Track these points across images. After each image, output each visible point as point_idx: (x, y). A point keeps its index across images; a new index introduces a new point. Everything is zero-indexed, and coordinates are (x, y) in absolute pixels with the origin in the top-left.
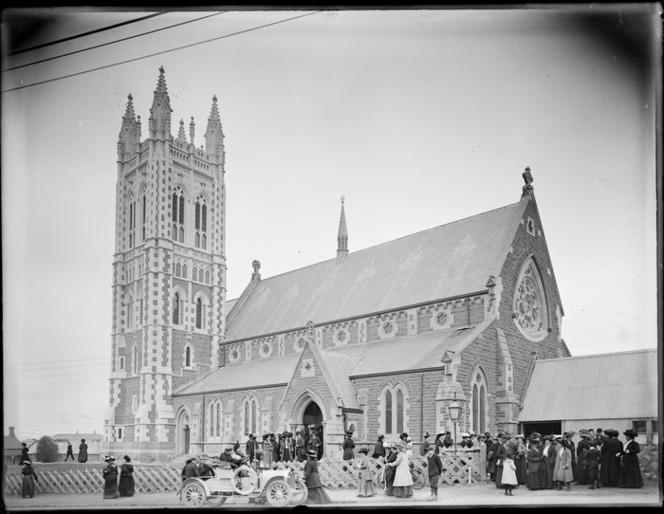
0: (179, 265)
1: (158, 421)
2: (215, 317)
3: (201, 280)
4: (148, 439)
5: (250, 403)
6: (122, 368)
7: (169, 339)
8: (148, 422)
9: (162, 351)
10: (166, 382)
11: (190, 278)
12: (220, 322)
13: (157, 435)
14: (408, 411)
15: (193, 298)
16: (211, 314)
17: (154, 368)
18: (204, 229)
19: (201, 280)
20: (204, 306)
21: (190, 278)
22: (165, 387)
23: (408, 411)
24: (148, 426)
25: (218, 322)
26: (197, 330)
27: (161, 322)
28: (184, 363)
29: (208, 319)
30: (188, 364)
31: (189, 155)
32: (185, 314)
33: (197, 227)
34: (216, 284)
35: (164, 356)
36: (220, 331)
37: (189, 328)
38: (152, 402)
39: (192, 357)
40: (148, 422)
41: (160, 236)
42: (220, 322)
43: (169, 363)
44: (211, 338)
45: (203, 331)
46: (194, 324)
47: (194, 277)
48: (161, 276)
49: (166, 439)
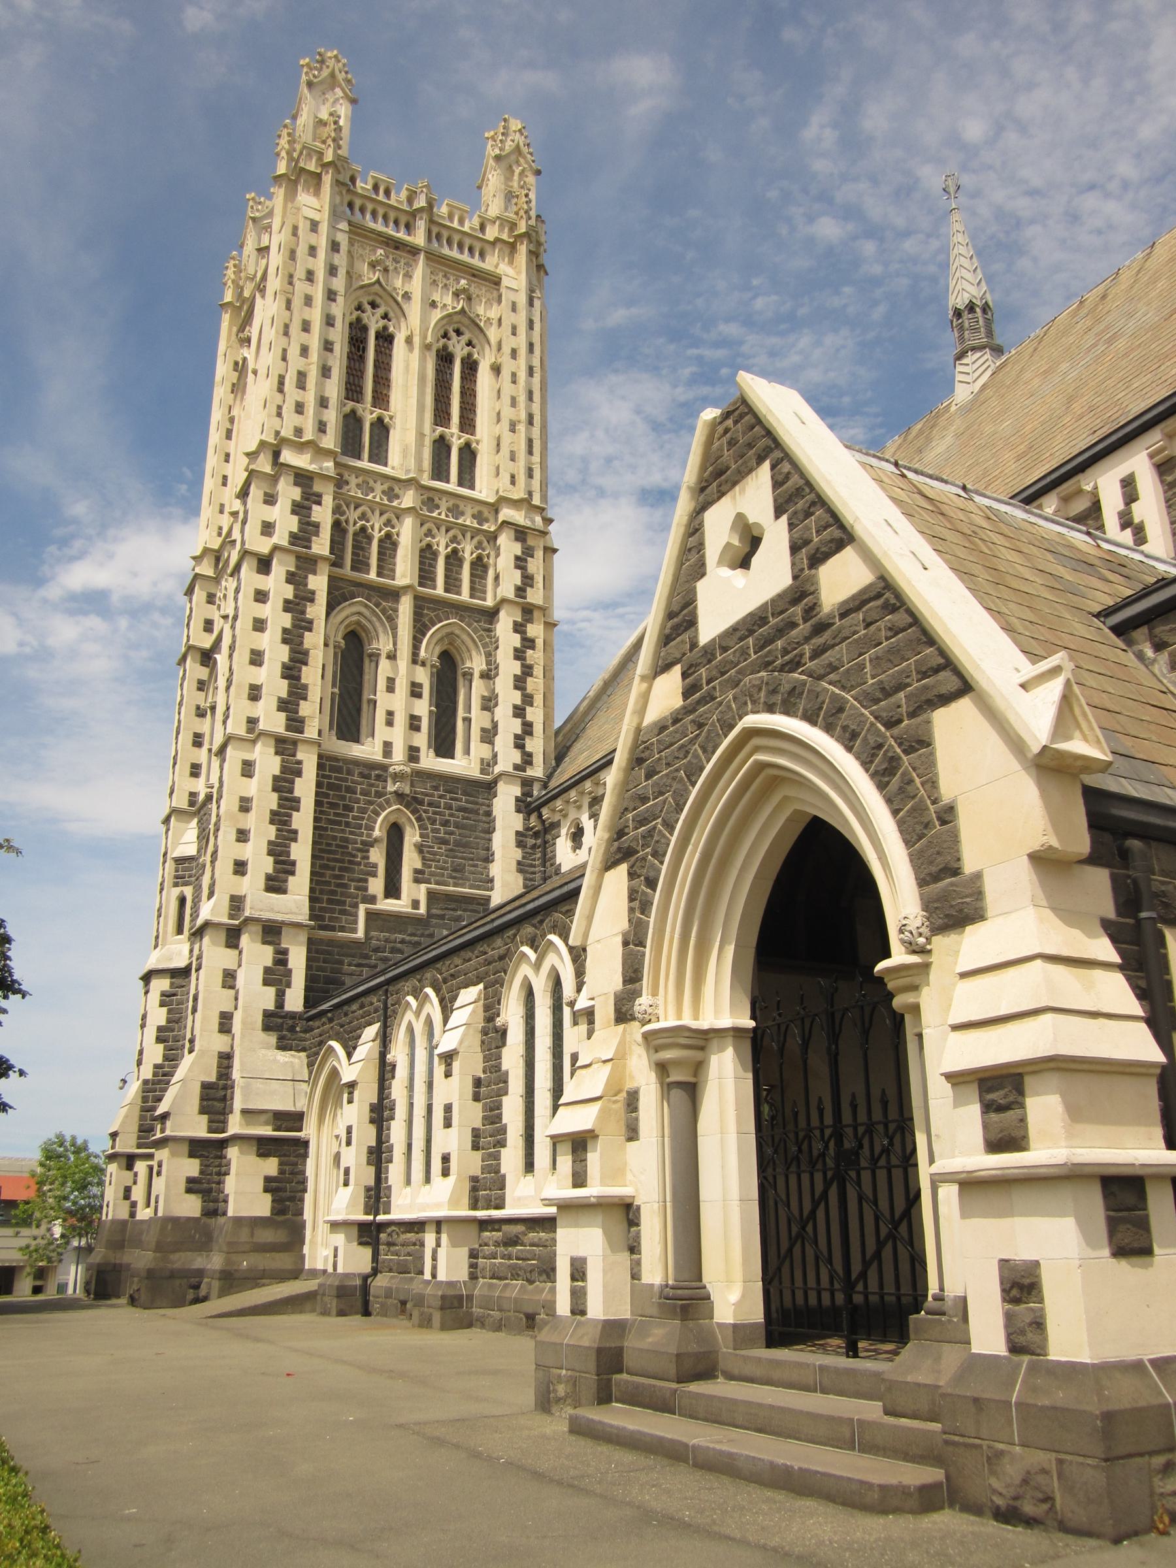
0: (363, 534)
1: (235, 1125)
2: (503, 712)
3: (452, 584)
4: (191, 1206)
5: (419, 1027)
6: (180, 931)
7: (305, 788)
8: (199, 1128)
9: (272, 832)
10: (281, 958)
11: (405, 571)
12: (528, 728)
13: (230, 1185)
14: (375, 875)
15: (416, 647)
16: (489, 703)
17: (237, 903)
18: (468, 423)
19: (452, 584)
20: (469, 676)
21: (405, 571)
22: (276, 976)
23: (375, 875)
24: (196, 1147)
25: (516, 726)
26: (430, 761)
27: (274, 722)
28: (376, 885)
29: (479, 719)
30: (392, 890)
31: (414, 214)
32: (384, 701)
33: (441, 415)
34: (510, 594)
35: (279, 851)
36: (528, 759)
37: (399, 754)
38: (220, 1043)
39: (410, 860)
40: (199, 1128)
41: (288, 433)
42: (528, 728)
43: (300, 883)
44: (489, 788)
45: (462, 765)
46: (421, 740)
47: (426, 575)
48: (280, 568)
49: (262, 1206)
